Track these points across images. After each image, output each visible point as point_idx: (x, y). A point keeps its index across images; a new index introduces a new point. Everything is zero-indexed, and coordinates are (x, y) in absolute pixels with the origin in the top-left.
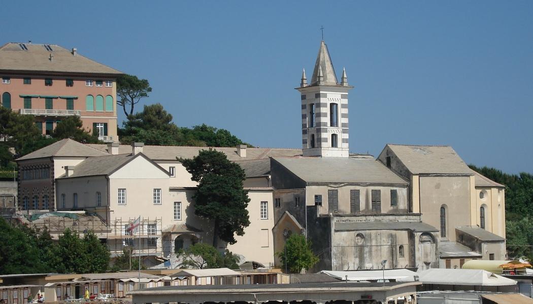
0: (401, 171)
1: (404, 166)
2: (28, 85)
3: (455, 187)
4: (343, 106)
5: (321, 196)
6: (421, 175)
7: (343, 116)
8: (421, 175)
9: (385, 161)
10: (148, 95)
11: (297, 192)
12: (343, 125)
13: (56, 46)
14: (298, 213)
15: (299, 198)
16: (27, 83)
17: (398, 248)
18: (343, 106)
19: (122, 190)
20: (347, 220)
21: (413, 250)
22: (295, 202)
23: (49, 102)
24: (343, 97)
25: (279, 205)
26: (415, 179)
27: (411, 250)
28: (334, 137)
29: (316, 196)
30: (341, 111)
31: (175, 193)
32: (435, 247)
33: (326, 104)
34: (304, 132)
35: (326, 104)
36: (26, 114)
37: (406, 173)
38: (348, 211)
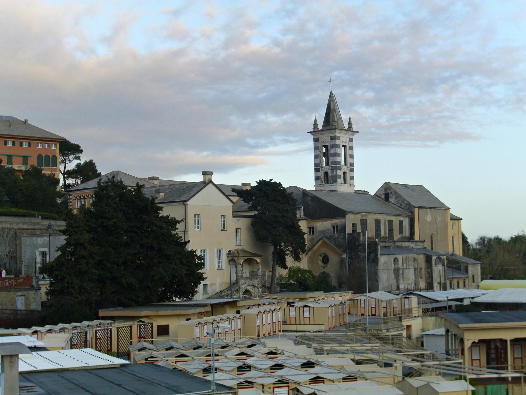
0: (401, 205)
1: (404, 200)
5: (356, 224)
6: (419, 208)
8: (419, 208)
9: (383, 197)
11: (338, 221)
14: (337, 240)
15: (337, 226)
17: (419, 269)
19: (197, 216)
21: (430, 272)
22: (332, 230)
25: (313, 233)
26: (416, 210)
27: (428, 273)
29: (353, 224)
31: (5, 369)
34: (317, 170)
37: (408, 206)
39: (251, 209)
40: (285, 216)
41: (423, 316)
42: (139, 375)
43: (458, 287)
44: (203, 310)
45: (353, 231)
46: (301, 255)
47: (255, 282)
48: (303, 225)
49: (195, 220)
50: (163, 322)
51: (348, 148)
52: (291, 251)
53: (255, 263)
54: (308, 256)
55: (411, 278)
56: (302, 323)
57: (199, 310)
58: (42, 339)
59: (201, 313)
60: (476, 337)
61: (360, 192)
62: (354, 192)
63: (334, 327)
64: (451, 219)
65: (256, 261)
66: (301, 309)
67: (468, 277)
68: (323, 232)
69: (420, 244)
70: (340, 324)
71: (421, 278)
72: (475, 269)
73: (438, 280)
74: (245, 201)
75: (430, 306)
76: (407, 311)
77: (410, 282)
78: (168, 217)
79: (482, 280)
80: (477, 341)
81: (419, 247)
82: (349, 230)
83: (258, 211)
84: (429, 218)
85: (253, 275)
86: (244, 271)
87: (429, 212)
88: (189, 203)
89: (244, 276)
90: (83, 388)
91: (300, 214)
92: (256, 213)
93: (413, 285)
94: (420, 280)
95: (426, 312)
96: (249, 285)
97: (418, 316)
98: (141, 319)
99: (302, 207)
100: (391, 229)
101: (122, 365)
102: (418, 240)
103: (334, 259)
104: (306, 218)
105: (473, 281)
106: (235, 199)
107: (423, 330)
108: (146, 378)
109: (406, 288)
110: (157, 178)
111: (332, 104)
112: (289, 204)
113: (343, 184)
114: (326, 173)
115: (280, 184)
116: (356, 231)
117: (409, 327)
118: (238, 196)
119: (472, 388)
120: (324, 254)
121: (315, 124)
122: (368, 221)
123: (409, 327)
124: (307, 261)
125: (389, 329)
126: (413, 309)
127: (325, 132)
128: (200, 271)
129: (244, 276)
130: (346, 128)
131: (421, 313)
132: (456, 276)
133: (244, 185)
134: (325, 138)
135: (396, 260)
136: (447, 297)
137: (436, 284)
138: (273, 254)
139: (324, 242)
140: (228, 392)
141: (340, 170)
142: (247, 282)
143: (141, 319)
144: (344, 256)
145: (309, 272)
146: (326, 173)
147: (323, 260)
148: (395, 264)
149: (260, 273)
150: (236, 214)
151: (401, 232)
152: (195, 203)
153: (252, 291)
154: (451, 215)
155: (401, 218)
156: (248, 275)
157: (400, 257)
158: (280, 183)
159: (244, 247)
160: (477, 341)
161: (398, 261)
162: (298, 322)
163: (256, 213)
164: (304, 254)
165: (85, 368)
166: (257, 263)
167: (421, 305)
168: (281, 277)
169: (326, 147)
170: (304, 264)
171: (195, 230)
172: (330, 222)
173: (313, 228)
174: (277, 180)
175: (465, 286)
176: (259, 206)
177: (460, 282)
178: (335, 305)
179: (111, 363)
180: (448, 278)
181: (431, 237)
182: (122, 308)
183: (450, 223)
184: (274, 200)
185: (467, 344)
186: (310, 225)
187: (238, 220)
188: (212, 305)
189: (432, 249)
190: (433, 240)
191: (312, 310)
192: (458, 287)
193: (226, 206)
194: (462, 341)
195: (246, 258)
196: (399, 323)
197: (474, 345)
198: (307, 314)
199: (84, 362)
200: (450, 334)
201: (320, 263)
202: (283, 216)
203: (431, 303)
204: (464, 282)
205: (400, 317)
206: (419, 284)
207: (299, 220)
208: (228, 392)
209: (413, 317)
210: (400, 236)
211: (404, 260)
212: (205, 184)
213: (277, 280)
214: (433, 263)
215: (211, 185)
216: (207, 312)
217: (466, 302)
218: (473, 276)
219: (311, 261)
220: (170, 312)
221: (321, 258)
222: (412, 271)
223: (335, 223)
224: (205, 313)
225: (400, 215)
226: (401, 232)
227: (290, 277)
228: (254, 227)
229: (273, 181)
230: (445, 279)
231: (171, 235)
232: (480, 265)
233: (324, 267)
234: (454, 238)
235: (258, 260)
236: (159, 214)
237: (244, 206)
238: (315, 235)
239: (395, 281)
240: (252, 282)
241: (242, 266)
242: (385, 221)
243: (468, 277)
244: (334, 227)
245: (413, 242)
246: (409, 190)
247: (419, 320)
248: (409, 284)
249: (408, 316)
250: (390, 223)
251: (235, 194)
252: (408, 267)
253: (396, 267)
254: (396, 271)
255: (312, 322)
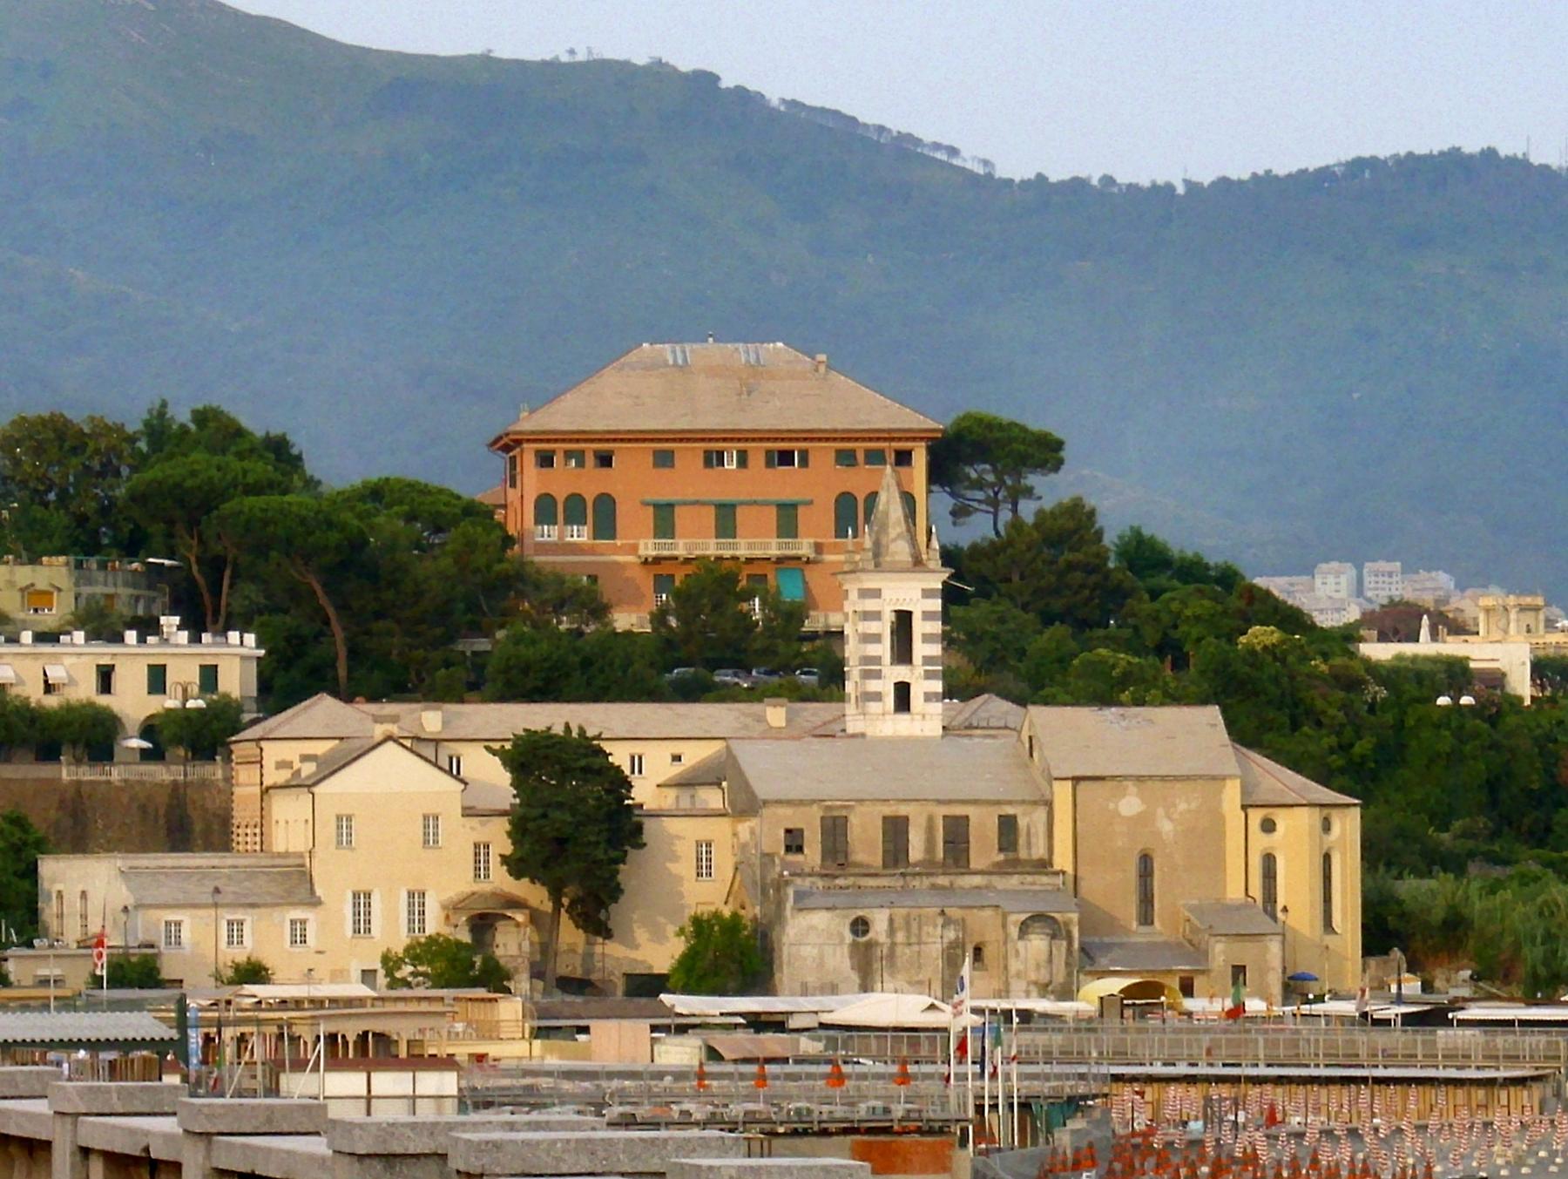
2: (666, 471)
3: (1182, 806)
4: (928, 616)
7: (927, 638)
10: (1037, 492)
12: (928, 660)
13: (780, 345)
16: (664, 466)
18: (928, 616)
20: (853, 886)
23: (726, 519)
24: (927, 594)
28: (903, 691)
29: (788, 831)
30: (919, 627)
32: (1064, 950)
36: (654, 553)
38: (877, 859)
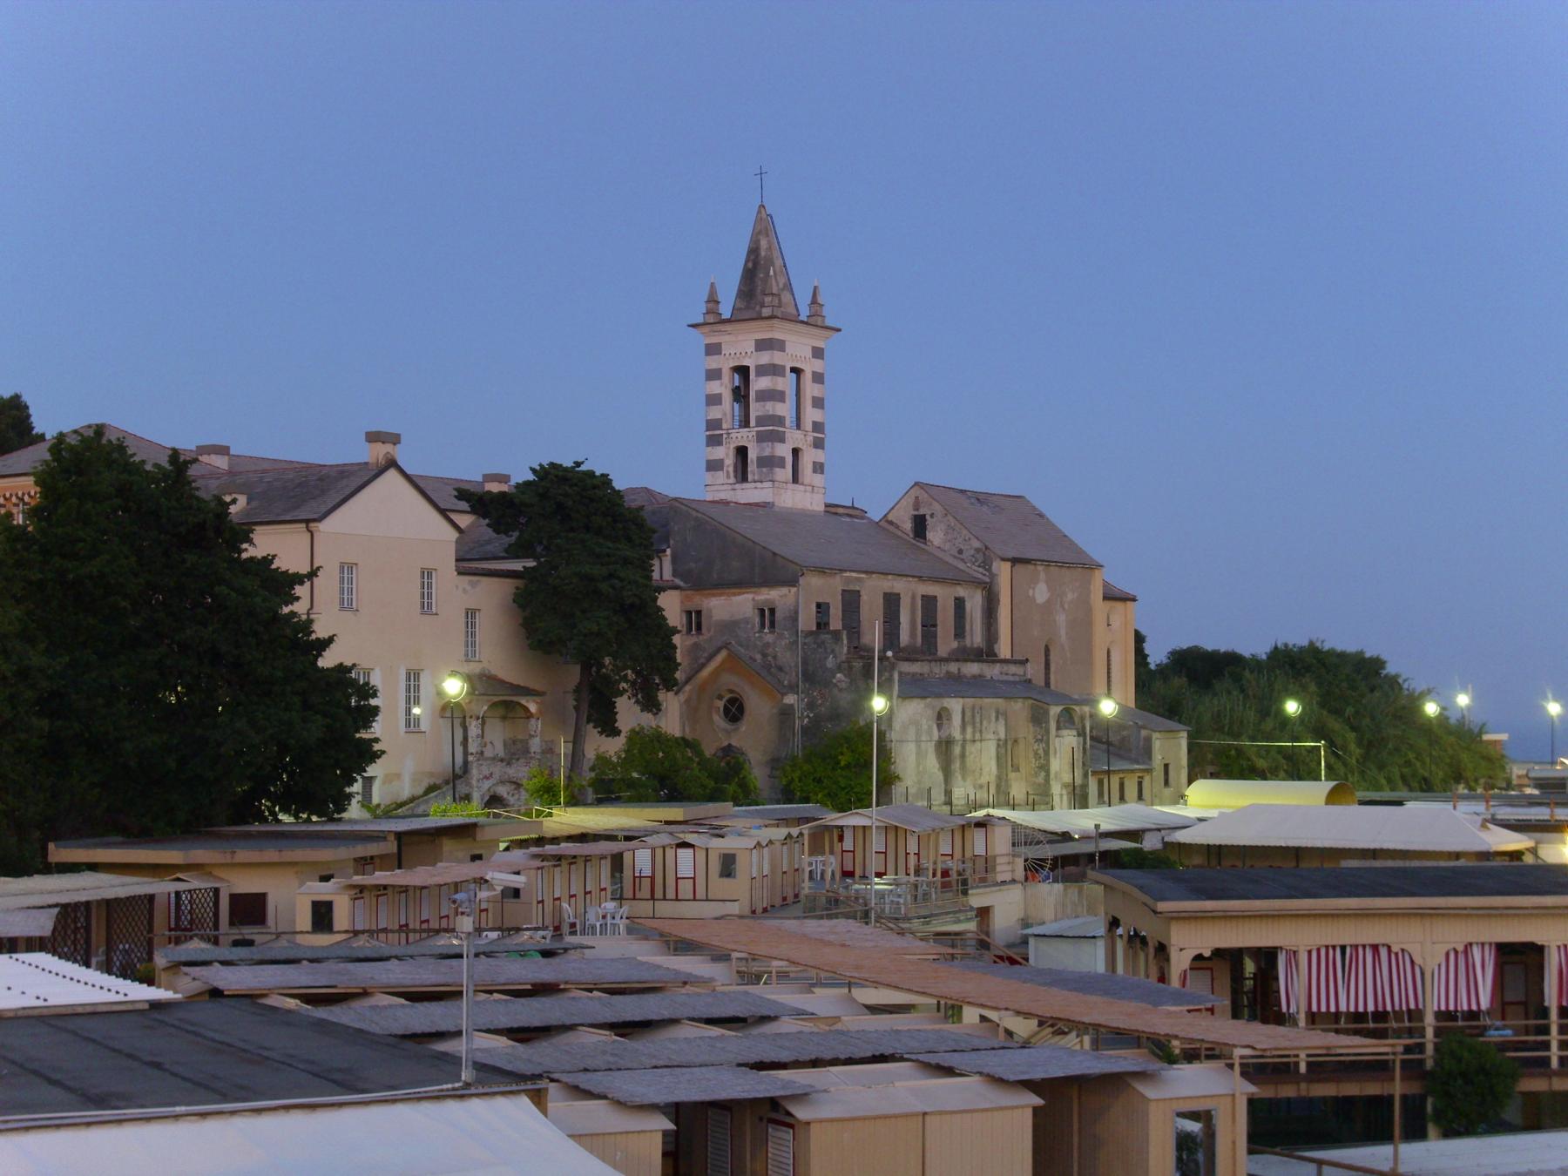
0: (960, 552)
6: (1015, 561)
9: (908, 526)
15: (772, 611)
19: (347, 568)
21: (1041, 752)
22: (757, 620)
25: (699, 627)
29: (819, 605)
33: (720, 370)
34: (714, 441)
35: (720, 370)
39: (513, 553)
40: (618, 578)
41: (1026, 879)
42: (217, 1036)
43: (1122, 799)
44: (373, 849)
45: (819, 625)
46: (662, 696)
47: (519, 771)
48: (671, 606)
49: (342, 580)
50: (247, 884)
51: (807, 377)
52: (633, 684)
53: (521, 713)
54: (682, 697)
55: (986, 771)
56: (671, 894)
57: (362, 850)
58: (460, 573)
59: (364, 859)
60: (1207, 939)
61: (841, 511)
62: (822, 508)
63: (765, 910)
64: (1106, 598)
65: (526, 709)
66: (670, 853)
67: (1149, 771)
68: (731, 626)
69: (1013, 669)
70: (784, 899)
71: (1016, 769)
72: (1172, 746)
73: (1067, 778)
74: (498, 527)
75: (1049, 851)
76: (980, 864)
77: (983, 780)
78: (267, 560)
79: (1190, 782)
80: (1207, 954)
81: (1011, 678)
82: (807, 620)
83: (536, 558)
84: (1041, 593)
85: (516, 751)
86: (488, 738)
87: (1042, 575)
88: (324, 527)
89: (488, 753)
90: (35, 1073)
91: (663, 569)
92: (531, 563)
93: (993, 790)
94: (1012, 775)
95: (1034, 868)
96: (502, 782)
97: (1013, 881)
98: (179, 875)
99: (669, 551)
100: (929, 624)
101: (156, 1005)
102: (1008, 656)
103: (759, 707)
104: (678, 582)
105: (1167, 783)
106: (465, 521)
107: (1025, 923)
108: (241, 1045)
109: (972, 797)
110: (223, 450)
111: (764, 243)
112: (629, 540)
113: (791, 486)
114: (742, 452)
115: (605, 480)
116: (827, 624)
117: (984, 913)
118: (473, 511)
119: (1252, 1089)
120: (731, 691)
121: (713, 300)
122: (864, 598)
123: (984, 913)
124: (677, 714)
125: (932, 915)
126: (999, 860)
127: (738, 326)
128: (363, 735)
129: (488, 753)
130: (803, 317)
131: (1020, 873)
132: (1118, 765)
133: (489, 478)
134: (740, 346)
135: (941, 717)
136: (1097, 826)
137: (1056, 789)
138: (577, 690)
139: (733, 656)
140: (514, 1087)
141: (782, 440)
142: (498, 770)
143: (179, 875)
144: (790, 699)
145: (685, 742)
146: (742, 452)
147: (727, 711)
148: (939, 726)
149: (535, 745)
150: (468, 562)
151: (960, 632)
152: (349, 524)
153: (512, 800)
154: (1106, 585)
155: (961, 592)
156: (500, 751)
157: (955, 705)
158: (604, 476)
159: (485, 664)
160: (1207, 954)
161: (949, 719)
162: (658, 894)
163: (531, 563)
164: (670, 694)
165: (36, 1012)
166: (528, 715)
167: (1022, 849)
168: (602, 760)
169: (743, 371)
170: (672, 718)
171: (342, 609)
172: (750, 596)
173: (699, 613)
174: (596, 465)
175: (1140, 797)
176: (540, 543)
177: (1127, 783)
178: (771, 842)
179: (120, 998)
180: (1094, 773)
181: (1047, 650)
182: (120, 839)
183: (1099, 607)
184: (587, 528)
185: (1180, 962)
186: (692, 606)
187: (473, 585)
188: (399, 836)
189: (1047, 684)
190: (1052, 657)
191: (701, 855)
192: (1122, 799)
193: (437, 537)
194: (1162, 950)
195: (496, 699)
196: (962, 898)
197: (1199, 964)
198: (686, 869)
199: (32, 992)
200: (1120, 931)
201: (719, 720)
202: (611, 576)
203: (1050, 842)
204: (1140, 784)
205: (965, 882)
206: (1008, 786)
207: (661, 589)
208: (514, 1087)
209: (997, 884)
210: (955, 645)
211: (968, 714)
212: (367, 475)
213: (592, 769)
214: (1053, 725)
215: (392, 474)
216: (382, 857)
217: (1150, 843)
218: (1166, 766)
219: (691, 712)
220: (271, 855)
221: (721, 704)
222: (990, 749)
223: (767, 601)
224: (377, 861)
225: (956, 582)
226: (960, 632)
227: (628, 759)
228: (522, 607)
229: (583, 468)
230: (1085, 775)
231: (276, 618)
232: (1185, 734)
233: (728, 732)
234: (1113, 654)
235: (533, 708)
236: (240, 551)
237: (489, 542)
238: (706, 635)
239: (940, 776)
240: (512, 772)
241: (483, 723)
242: (913, 598)
243: (1149, 771)
244: (762, 611)
245: (994, 662)
246: (985, 508)
247: (1015, 895)
248: (981, 787)
249: (983, 880)
250: (929, 602)
251: (464, 505)
252: (977, 736)
253: (944, 734)
254: (945, 747)
255: (701, 893)
